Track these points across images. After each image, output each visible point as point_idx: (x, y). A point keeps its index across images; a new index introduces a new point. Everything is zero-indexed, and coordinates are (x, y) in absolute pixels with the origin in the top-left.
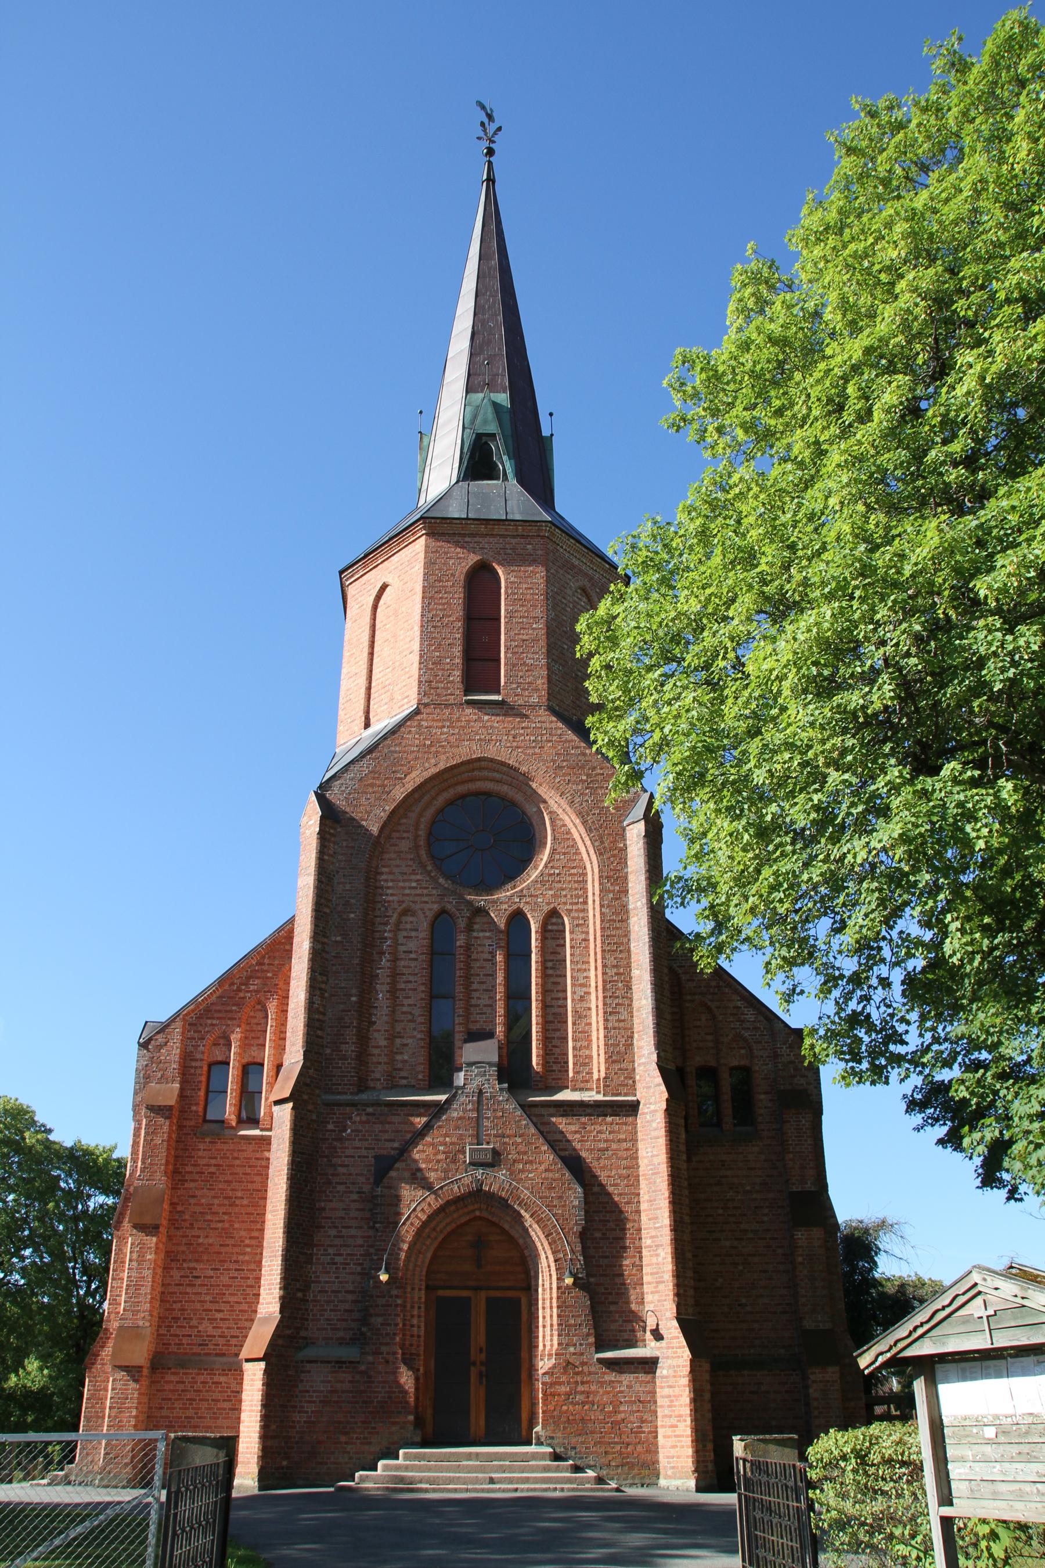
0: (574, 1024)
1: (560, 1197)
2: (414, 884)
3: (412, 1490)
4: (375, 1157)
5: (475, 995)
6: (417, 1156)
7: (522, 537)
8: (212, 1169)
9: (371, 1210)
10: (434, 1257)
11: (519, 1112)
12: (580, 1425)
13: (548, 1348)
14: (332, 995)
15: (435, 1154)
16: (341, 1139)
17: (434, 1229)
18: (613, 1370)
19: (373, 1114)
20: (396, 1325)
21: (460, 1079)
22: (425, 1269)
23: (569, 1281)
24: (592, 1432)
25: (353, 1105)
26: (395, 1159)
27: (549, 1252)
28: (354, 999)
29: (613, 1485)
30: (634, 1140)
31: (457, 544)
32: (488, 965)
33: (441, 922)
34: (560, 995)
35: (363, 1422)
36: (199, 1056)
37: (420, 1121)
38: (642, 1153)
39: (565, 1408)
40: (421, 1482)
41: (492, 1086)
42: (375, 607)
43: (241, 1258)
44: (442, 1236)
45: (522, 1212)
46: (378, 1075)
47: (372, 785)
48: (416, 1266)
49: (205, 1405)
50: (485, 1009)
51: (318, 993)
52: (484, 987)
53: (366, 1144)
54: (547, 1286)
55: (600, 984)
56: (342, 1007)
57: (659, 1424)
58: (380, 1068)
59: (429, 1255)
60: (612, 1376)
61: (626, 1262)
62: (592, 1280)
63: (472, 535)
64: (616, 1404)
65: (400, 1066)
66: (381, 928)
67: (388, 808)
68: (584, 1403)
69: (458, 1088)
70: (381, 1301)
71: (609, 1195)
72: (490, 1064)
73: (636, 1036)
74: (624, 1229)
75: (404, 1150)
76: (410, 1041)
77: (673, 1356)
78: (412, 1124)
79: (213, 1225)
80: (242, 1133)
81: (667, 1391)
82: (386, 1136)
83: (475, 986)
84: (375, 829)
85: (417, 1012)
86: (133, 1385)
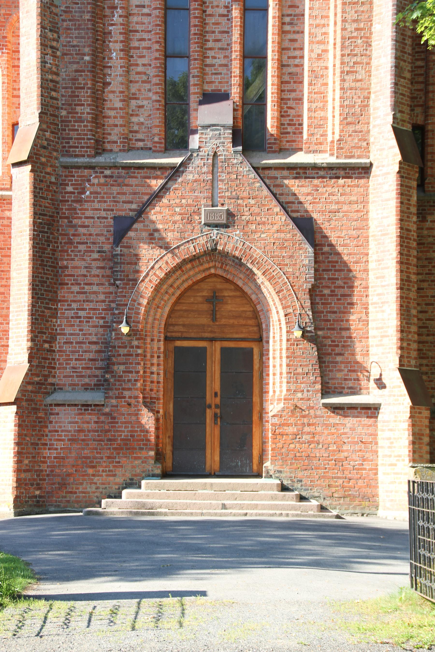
0: (310, 84)
1: (291, 257)
3: (153, 514)
4: (115, 218)
5: (210, 53)
6: (153, 217)
9: (111, 268)
10: (172, 311)
11: (253, 174)
12: (307, 461)
13: (277, 393)
14: (64, 54)
15: (172, 215)
17: (171, 286)
19: (111, 177)
20: (138, 372)
21: (194, 142)
22: (163, 323)
23: (298, 334)
25: (92, 167)
26: (134, 220)
27: (280, 308)
28: (87, 58)
29: (335, 513)
30: (365, 202)
32: (223, 20)
34: (297, 53)
35: (109, 457)
37: (156, 184)
38: (371, 215)
39: (292, 446)
40: (160, 507)
41: (227, 149)
44: (179, 292)
45: (255, 270)
46: (113, 138)
48: (155, 319)
50: (220, 69)
51: (49, 51)
52: (219, 45)
53: (104, 206)
54: (277, 338)
55: (339, 40)
56: (75, 67)
57: (380, 462)
58: (116, 130)
59: (167, 309)
60: (336, 419)
61: (352, 317)
62: (320, 333)
64: (339, 445)
65: (136, 128)
69: (193, 151)
70: (122, 351)
72: (224, 127)
73: (372, 96)
74: (352, 287)
75: (141, 212)
76: (145, 103)
77: (395, 403)
78: (149, 186)
82: (124, 198)
83: (210, 44)
85: (152, 72)
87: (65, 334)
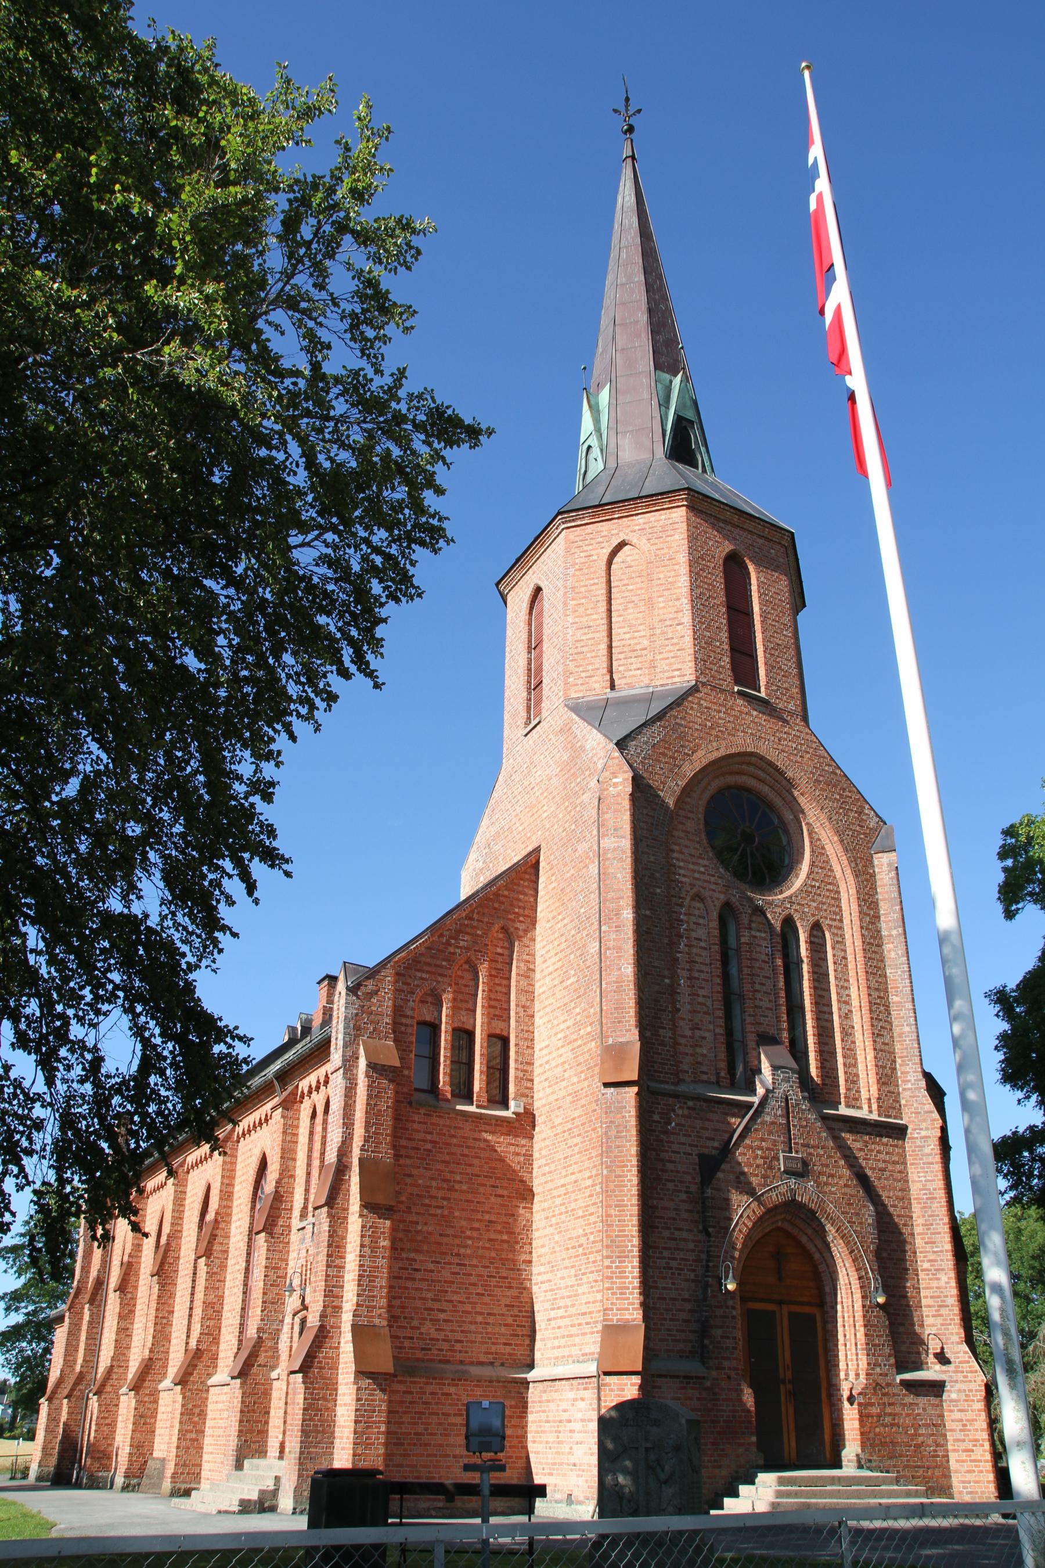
1: (858, 1214)
2: (702, 869)
4: (700, 1155)
7: (767, 539)
8: (429, 1146)
16: (666, 1132)
18: (911, 1392)
19: (694, 1109)
24: (901, 1456)
31: (714, 526)
33: (727, 913)
35: (713, 1444)
36: (409, 1013)
42: (610, 563)
43: (462, 1250)
47: (664, 755)
49: (434, 1419)
52: (764, 989)
56: (657, 988)
57: (950, 1447)
60: (910, 1399)
63: (725, 522)
66: (676, 909)
67: (682, 783)
68: (892, 1425)
70: (719, 1312)
71: (890, 1215)
76: (707, 1034)
78: (729, 1123)
79: (432, 1211)
80: (459, 1107)
81: (957, 1415)
82: (707, 1134)
84: (671, 802)
86: (379, 1395)
87: (657, 1288)
